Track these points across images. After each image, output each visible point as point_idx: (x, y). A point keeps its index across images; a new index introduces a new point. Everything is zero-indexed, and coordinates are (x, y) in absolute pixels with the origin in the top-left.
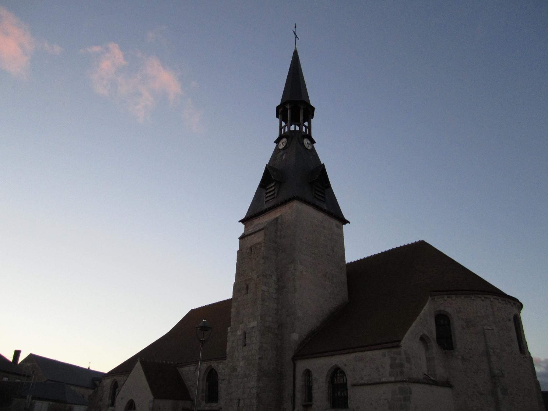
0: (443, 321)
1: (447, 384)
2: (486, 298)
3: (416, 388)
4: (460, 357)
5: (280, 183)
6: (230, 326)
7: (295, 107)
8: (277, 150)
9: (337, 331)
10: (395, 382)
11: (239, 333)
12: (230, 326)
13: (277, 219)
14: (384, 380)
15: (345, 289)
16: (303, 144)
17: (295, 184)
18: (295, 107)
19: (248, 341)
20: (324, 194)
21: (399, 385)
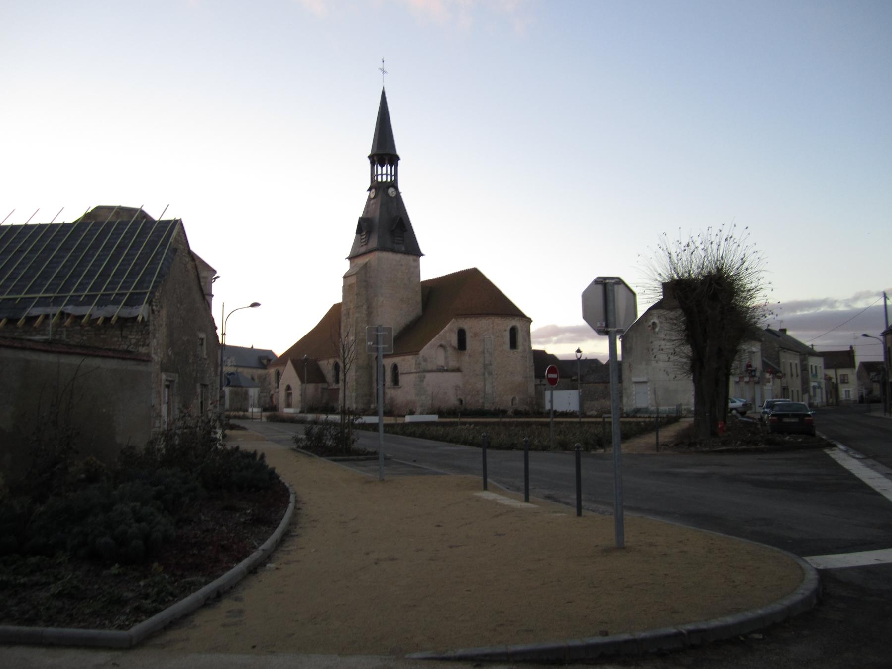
0: (462, 334)
1: (458, 370)
3: (428, 375)
5: (369, 233)
7: (384, 152)
8: (369, 199)
9: (409, 338)
13: (366, 264)
15: (420, 306)
16: (387, 195)
17: (386, 227)
18: (384, 152)
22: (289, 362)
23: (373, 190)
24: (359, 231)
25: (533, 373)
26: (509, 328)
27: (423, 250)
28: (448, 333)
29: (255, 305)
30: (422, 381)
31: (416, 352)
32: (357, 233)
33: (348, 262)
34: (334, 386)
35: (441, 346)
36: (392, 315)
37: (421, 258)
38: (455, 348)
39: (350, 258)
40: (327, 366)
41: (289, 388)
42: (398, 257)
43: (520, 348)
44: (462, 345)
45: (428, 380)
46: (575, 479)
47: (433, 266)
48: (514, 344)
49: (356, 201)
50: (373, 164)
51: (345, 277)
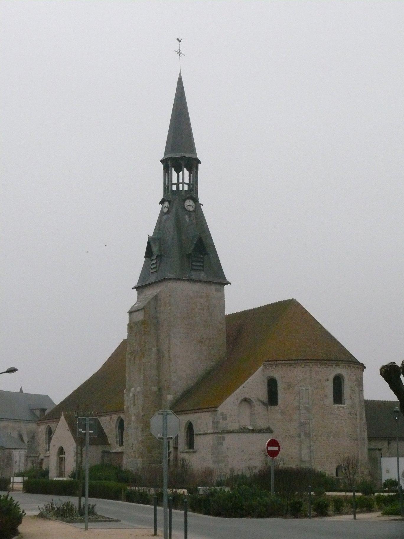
0: (272, 384)
2: (307, 365)
3: (229, 437)
4: (280, 411)
6: (125, 388)
8: (162, 214)
10: (214, 433)
11: (131, 395)
12: (125, 388)
14: (209, 432)
17: (182, 247)
19: (136, 402)
20: (203, 262)
21: (216, 435)
22: (63, 417)
23: (166, 204)
24: (149, 253)
25: (366, 435)
26: (331, 377)
27: (228, 278)
28: (254, 385)
29: (12, 370)
30: (221, 444)
31: (212, 408)
32: (146, 256)
33: (135, 292)
34: (119, 449)
35: (246, 400)
36: (185, 362)
37: (226, 287)
38: (263, 403)
39: (137, 288)
40: (108, 424)
41: (61, 451)
42: (196, 287)
43: (347, 402)
44: (272, 398)
45: (230, 444)
46: (172, 526)
47: (240, 297)
48: (338, 398)
49: (145, 215)
50: (167, 170)
51: (130, 313)
